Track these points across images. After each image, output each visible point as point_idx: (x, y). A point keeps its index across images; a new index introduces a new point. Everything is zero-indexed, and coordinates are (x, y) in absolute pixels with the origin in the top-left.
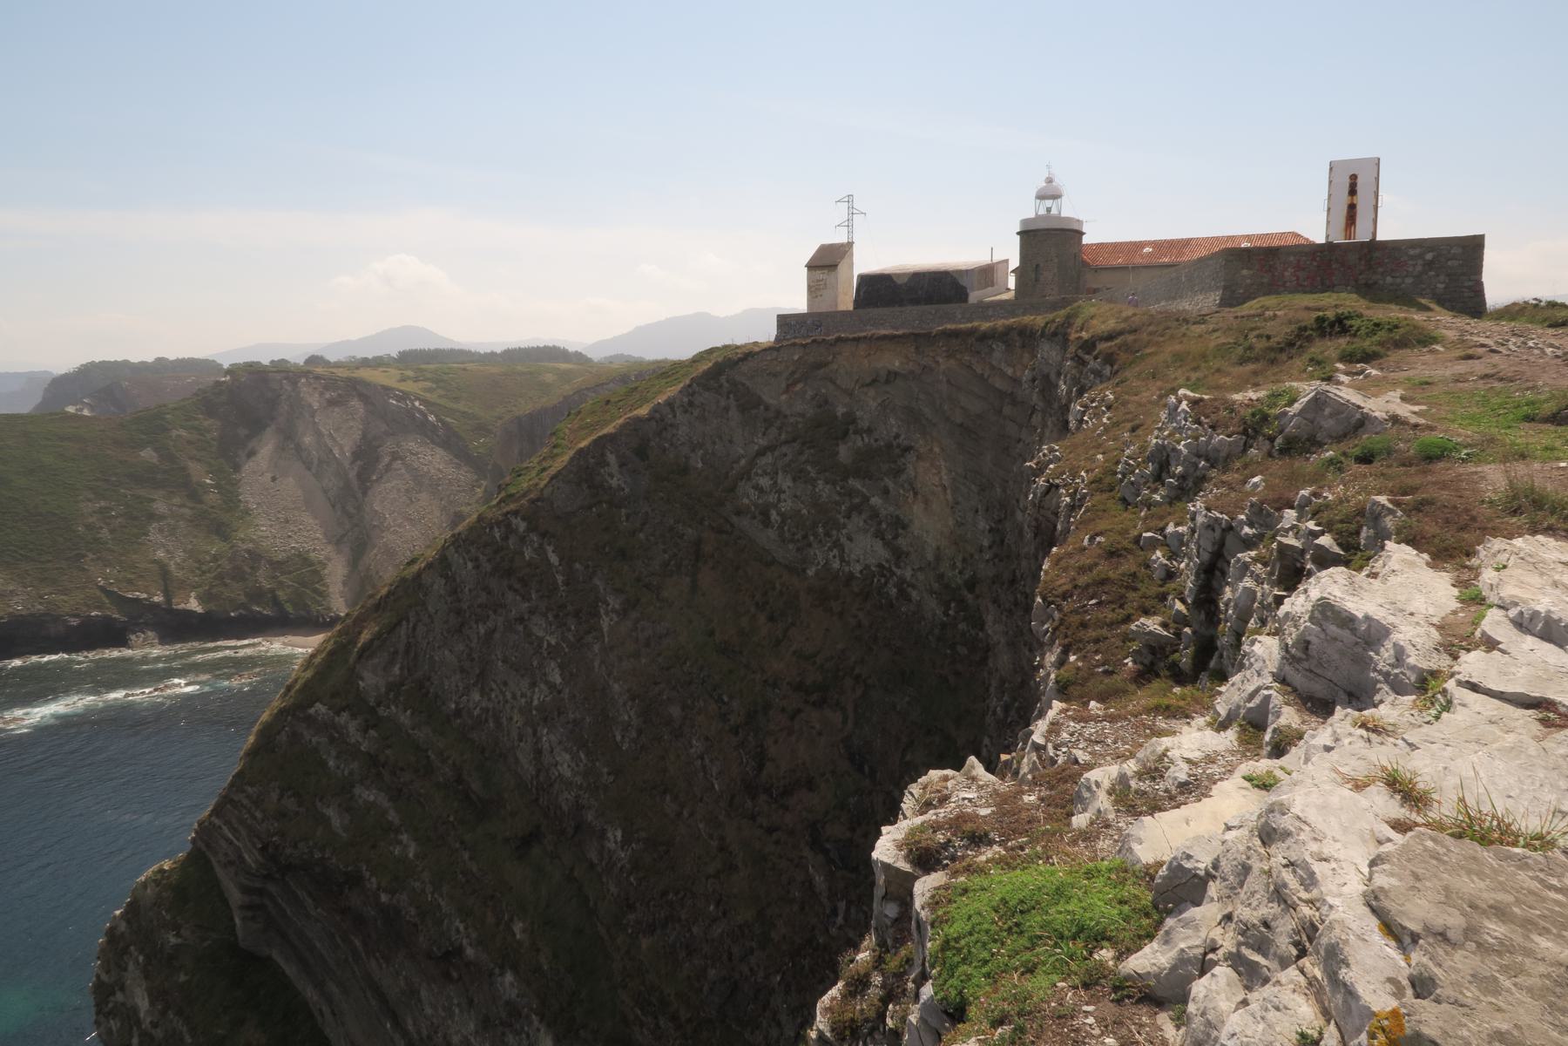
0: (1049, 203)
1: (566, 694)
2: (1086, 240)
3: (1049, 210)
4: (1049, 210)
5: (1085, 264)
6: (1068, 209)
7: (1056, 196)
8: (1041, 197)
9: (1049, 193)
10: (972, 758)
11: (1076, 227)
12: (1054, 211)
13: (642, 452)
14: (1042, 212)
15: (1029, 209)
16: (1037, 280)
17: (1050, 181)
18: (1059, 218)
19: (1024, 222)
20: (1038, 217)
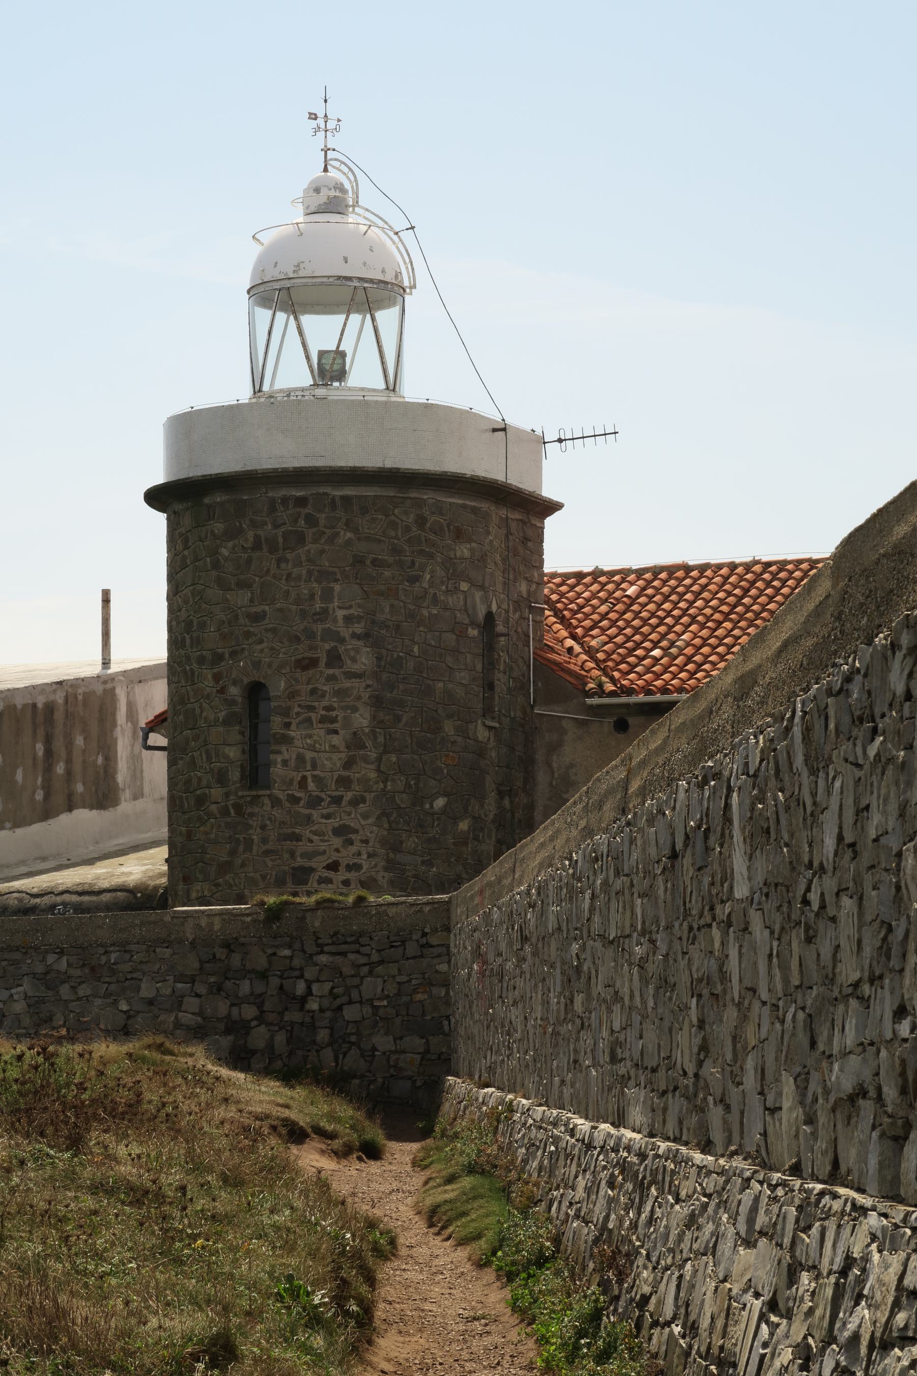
0: (323, 330)
1: (822, 765)
2: (565, 548)
3: (331, 368)
4: (331, 368)
5: (557, 682)
6: (457, 361)
7: (369, 293)
8: (283, 293)
9: (322, 283)
10: (271, 756)
11: (484, 464)
12: (364, 375)
13: (319, 1172)
14: (293, 374)
15: (211, 359)
16: (255, 774)
17: (330, 202)
18: (388, 409)
19: (186, 428)
20: (266, 403)
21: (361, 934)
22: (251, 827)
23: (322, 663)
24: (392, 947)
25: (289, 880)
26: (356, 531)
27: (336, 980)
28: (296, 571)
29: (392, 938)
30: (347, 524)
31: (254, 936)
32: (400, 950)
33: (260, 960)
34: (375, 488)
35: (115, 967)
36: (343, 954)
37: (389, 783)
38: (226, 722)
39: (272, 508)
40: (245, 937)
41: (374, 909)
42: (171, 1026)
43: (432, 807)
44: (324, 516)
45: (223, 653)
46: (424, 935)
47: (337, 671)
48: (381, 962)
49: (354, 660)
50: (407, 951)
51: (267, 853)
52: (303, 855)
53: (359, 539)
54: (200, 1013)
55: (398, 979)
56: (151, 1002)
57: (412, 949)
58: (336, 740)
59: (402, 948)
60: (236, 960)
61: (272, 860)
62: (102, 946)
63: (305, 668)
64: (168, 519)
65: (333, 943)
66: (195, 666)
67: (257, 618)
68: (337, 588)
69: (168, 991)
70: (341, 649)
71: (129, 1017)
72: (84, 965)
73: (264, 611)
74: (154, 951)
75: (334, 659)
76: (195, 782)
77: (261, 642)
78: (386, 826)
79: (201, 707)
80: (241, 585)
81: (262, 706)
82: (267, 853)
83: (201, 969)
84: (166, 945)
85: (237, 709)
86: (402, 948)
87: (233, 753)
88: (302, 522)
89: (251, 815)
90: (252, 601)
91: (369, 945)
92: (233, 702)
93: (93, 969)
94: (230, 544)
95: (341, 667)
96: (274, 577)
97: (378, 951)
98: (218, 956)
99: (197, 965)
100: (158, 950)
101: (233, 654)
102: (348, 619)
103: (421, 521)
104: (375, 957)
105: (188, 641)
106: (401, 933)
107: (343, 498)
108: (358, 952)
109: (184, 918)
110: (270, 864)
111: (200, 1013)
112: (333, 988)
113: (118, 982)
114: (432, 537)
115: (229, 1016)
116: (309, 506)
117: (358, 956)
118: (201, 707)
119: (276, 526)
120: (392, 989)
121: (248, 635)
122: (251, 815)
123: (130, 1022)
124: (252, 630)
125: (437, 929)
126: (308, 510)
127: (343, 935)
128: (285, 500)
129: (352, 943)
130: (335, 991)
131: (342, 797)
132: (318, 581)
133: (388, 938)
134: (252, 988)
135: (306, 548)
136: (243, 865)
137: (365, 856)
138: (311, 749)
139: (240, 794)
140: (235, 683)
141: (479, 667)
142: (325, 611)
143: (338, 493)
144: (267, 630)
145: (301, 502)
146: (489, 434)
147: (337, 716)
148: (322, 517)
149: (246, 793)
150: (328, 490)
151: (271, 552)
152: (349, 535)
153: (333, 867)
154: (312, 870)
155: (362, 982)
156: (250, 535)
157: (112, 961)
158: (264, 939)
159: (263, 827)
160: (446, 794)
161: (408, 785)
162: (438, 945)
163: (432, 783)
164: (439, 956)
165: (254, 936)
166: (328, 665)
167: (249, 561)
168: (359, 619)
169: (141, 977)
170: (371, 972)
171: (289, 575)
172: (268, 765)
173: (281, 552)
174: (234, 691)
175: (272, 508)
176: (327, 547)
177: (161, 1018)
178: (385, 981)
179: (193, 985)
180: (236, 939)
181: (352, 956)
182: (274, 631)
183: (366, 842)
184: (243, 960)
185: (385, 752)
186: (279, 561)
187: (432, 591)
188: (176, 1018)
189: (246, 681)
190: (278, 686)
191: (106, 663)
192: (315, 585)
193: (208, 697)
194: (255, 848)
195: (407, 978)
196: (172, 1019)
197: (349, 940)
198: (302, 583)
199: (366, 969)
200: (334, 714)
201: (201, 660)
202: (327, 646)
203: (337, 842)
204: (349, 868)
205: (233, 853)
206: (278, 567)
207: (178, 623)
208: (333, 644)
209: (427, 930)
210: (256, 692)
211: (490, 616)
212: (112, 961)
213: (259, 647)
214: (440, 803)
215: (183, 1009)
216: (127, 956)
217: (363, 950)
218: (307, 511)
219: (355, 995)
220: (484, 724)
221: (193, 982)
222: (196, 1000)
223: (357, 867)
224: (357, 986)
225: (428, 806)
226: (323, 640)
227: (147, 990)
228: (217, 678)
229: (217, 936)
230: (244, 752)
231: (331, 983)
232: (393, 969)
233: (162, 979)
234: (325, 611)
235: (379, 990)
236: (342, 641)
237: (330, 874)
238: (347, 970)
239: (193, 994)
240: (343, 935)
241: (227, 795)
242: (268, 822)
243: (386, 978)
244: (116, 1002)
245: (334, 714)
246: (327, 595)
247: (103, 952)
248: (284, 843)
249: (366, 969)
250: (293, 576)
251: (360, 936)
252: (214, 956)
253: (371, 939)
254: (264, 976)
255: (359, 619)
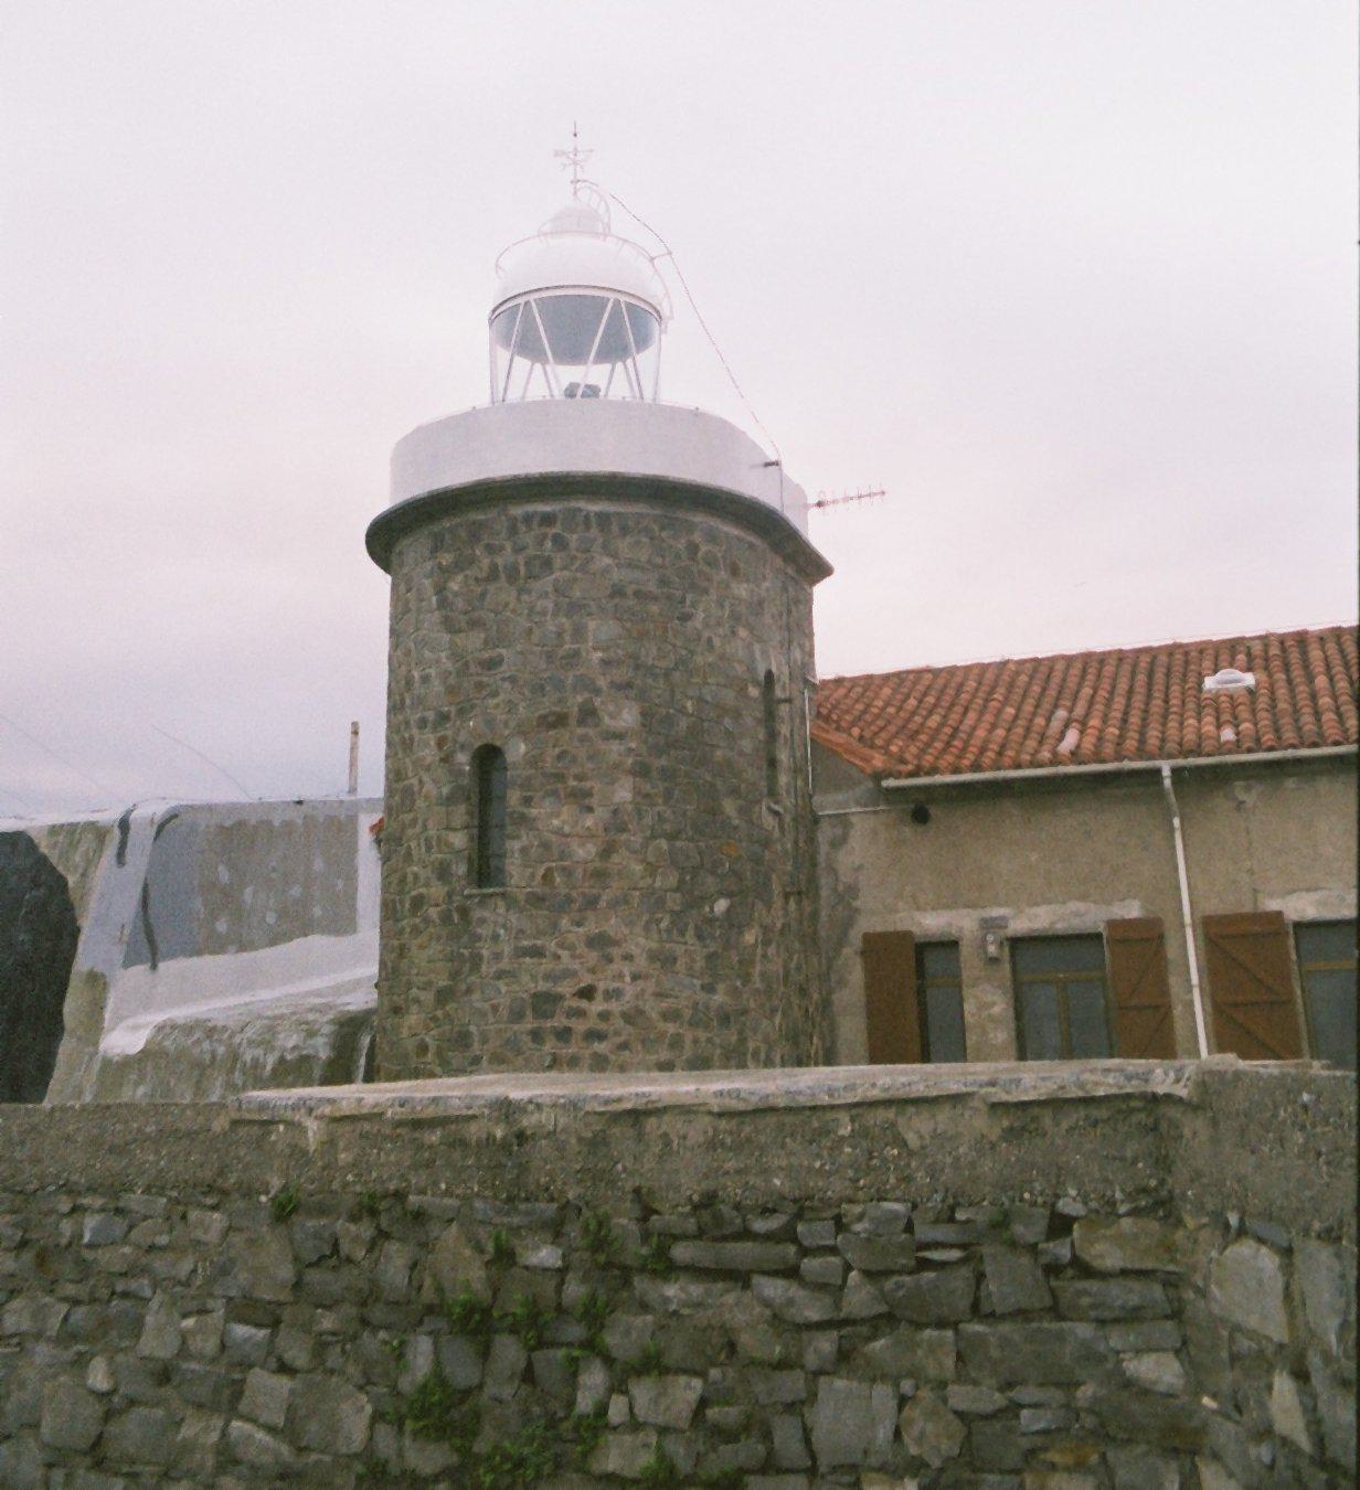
6: (727, 393)
16: (485, 869)
21: (802, 1208)
22: (479, 938)
23: (573, 721)
24: (925, 1264)
25: (529, 1013)
26: (614, 556)
27: (714, 1373)
28: (540, 604)
29: (924, 1232)
30: (604, 546)
31: (448, 1193)
32: (960, 1281)
33: (467, 1274)
34: (641, 505)
35: (88, 1255)
36: (739, 1277)
37: (658, 878)
38: (450, 800)
39: (513, 530)
40: (422, 1192)
41: (844, 1117)
42: (210, 1462)
43: (712, 910)
44: (575, 536)
45: (449, 712)
46: (1060, 1225)
47: (591, 732)
48: (886, 1320)
49: (612, 716)
50: (992, 1286)
51: (500, 975)
52: (547, 977)
53: (617, 565)
54: (289, 1431)
55: (961, 1397)
56: (164, 1375)
57: (1009, 1281)
58: (589, 821)
59: (965, 1272)
60: (395, 1264)
61: (507, 985)
62: (70, 1192)
63: (553, 726)
64: (394, 587)
65: (700, 1234)
66: (415, 731)
67: (491, 664)
68: (592, 625)
69: (210, 1345)
70: (597, 702)
71: (108, 1416)
72: (24, 1244)
73: (500, 655)
74: (184, 1217)
75: (588, 714)
76: (410, 878)
77: (495, 694)
78: (656, 937)
79: (421, 781)
80: (475, 624)
81: (495, 776)
82: (500, 975)
83: (298, 1285)
84: (209, 1201)
85: (465, 781)
86: (965, 1272)
87: (459, 840)
88: (549, 544)
89: (483, 921)
90: (486, 642)
91: (833, 1250)
92: (460, 773)
93: (42, 1259)
94: (460, 578)
95: (597, 725)
96: (513, 611)
97: (869, 1274)
98: (345, 1248)
99: (286, 1272)
100: (194, 1215)
101: (461, 712)
102: (606, 663)
103: (693, 549)
104: (859, 1298)
105: (408, 702)
106: (961, 1215)
107: (599, 515)
108: (791, 1273)
109: (264, 1123)
110: (504, 989)
111: (289, 1431)
112: (703, 1403)
113: (93, 1300)
114: (707, 569)
115: (368, 1454)
116: (558, 524)
117: (795, 1291)
118: (421, 781)
119: (518, 550)
120: (933, 1438)
121: (480, 686)
122: (483, 921)
123: (113, 1429)
124: (485, 679)
125: (1112, 1203)
126: (557, 529)
127: (737, 1207)
128: (528, 519)
129: (769, 1237)
130: (712, 1413)
131: (600, 896)
132: (568, 615)
133: (909, 1228)
134: (437, 1362)
135: (553, 576)
136: (469, 991)
137: (628, 979)
138: (554, 829)
139: (466, 892)
140: (462, 747)
141: (761, 737)
142: (576, 654)
143: (595, 507)
144: (503, 679)
145: (548, 520)
146: (762, 470)
147: (592, 788)
148: (573, 539)
149: (475, 891)
150: (581, 504)
151: (511, 584)
152: (607, 561)
153: (587, 993)
154: (561, 997)
155: (813, 1397)
156: (486, 562)
157: (86, 1239)
158: (478, 1204)
159: (495, 938)
160: (729, 895)
161: (681, 881)
162: (1124, 1273)
163: (710, 880)
164: (1132, 1316)
165: (448, 1193)
166: (582, 722)
167: (483, 595)
168: (619, 663)
169: (147, 1293)
170: (844, 1356)
171: (531, 610)
172: (502, 856)
173: (521, 581)
174: (463, 758)
175: (513, 530)
176: (579, 575)
177: (186, 1432)
178: (903, 1401)
179: (273, 1335)
180: (399, 1196)
181: (773, 1288)
182: (513, 680)
183: (628, 957)
184: (414, 1266)
185: (654, 837)
186: (521, 591)
187: (706, 634)
188: (224, 1434)
189: (478, 744)
190: (517, 751)
191: (353, 790)
192: (564, 620)
193: (428, 769)
194: (484, 968)
195: (999, 1400)
196: (214, 1437)
197: (760, 1225)
198: (548, 618)
199: (825, 1344)
200: (588, 784)
201: (423, 723)
202: (580, 699)
203: (593, 957)
204: (608, 995)
205: (454, 975)
206: (518, 599)
207: (397, 682)
208: (587, 695)
209: (1069, 1205)
210: (488, 757)
211: (769, 674)
212: (86, 1239)
213: (495, 701)
214: (721, 905)
215: (243, 1407)
216: (120, 1225)
217: (810, 1265)
218: (554, 531)
219: (786, 1437)
220: (769, 808)
221: (275, 1323)
222: (284, 1383)
223: (615, 994)
224: (791, 1407)
225: (707, 909)
226: (575, 689)
227: (156, 1343)
228: (441, 743)
229: (345, 1185)
230: (471, 839)
231: (697, 1383)
232: (935, 1349)
233: (194, 1305)
234: (576, 654)
235: (883, 1433)
236: (598, 692)
237: (584, 1004)
238: (757, 1342)
239: (273, 1363)
240: (737, 1207)
241: (450, 895)
242: (502, 932)
243: (907, 1386)
244: (81, 1363)
245: (588, 784)
246: (579, 633)
247: (65, 1207)
248: (521, 960)
249: (825, 1344)
250: (538, 609)
251: (799, 1216)
252: (336, 1246)
253: (840, 1225)
254: (477, 1324)
255: (619, 663)
